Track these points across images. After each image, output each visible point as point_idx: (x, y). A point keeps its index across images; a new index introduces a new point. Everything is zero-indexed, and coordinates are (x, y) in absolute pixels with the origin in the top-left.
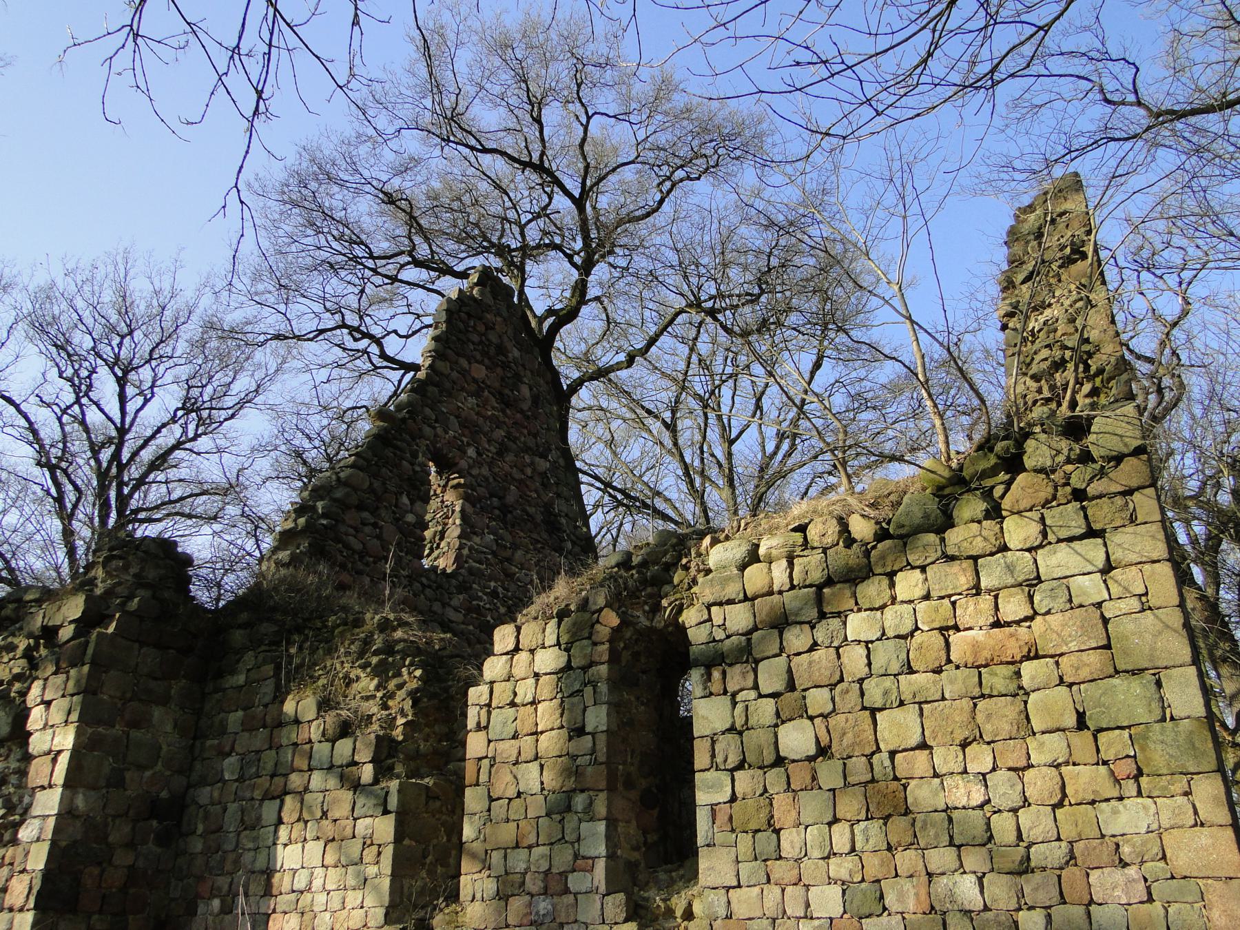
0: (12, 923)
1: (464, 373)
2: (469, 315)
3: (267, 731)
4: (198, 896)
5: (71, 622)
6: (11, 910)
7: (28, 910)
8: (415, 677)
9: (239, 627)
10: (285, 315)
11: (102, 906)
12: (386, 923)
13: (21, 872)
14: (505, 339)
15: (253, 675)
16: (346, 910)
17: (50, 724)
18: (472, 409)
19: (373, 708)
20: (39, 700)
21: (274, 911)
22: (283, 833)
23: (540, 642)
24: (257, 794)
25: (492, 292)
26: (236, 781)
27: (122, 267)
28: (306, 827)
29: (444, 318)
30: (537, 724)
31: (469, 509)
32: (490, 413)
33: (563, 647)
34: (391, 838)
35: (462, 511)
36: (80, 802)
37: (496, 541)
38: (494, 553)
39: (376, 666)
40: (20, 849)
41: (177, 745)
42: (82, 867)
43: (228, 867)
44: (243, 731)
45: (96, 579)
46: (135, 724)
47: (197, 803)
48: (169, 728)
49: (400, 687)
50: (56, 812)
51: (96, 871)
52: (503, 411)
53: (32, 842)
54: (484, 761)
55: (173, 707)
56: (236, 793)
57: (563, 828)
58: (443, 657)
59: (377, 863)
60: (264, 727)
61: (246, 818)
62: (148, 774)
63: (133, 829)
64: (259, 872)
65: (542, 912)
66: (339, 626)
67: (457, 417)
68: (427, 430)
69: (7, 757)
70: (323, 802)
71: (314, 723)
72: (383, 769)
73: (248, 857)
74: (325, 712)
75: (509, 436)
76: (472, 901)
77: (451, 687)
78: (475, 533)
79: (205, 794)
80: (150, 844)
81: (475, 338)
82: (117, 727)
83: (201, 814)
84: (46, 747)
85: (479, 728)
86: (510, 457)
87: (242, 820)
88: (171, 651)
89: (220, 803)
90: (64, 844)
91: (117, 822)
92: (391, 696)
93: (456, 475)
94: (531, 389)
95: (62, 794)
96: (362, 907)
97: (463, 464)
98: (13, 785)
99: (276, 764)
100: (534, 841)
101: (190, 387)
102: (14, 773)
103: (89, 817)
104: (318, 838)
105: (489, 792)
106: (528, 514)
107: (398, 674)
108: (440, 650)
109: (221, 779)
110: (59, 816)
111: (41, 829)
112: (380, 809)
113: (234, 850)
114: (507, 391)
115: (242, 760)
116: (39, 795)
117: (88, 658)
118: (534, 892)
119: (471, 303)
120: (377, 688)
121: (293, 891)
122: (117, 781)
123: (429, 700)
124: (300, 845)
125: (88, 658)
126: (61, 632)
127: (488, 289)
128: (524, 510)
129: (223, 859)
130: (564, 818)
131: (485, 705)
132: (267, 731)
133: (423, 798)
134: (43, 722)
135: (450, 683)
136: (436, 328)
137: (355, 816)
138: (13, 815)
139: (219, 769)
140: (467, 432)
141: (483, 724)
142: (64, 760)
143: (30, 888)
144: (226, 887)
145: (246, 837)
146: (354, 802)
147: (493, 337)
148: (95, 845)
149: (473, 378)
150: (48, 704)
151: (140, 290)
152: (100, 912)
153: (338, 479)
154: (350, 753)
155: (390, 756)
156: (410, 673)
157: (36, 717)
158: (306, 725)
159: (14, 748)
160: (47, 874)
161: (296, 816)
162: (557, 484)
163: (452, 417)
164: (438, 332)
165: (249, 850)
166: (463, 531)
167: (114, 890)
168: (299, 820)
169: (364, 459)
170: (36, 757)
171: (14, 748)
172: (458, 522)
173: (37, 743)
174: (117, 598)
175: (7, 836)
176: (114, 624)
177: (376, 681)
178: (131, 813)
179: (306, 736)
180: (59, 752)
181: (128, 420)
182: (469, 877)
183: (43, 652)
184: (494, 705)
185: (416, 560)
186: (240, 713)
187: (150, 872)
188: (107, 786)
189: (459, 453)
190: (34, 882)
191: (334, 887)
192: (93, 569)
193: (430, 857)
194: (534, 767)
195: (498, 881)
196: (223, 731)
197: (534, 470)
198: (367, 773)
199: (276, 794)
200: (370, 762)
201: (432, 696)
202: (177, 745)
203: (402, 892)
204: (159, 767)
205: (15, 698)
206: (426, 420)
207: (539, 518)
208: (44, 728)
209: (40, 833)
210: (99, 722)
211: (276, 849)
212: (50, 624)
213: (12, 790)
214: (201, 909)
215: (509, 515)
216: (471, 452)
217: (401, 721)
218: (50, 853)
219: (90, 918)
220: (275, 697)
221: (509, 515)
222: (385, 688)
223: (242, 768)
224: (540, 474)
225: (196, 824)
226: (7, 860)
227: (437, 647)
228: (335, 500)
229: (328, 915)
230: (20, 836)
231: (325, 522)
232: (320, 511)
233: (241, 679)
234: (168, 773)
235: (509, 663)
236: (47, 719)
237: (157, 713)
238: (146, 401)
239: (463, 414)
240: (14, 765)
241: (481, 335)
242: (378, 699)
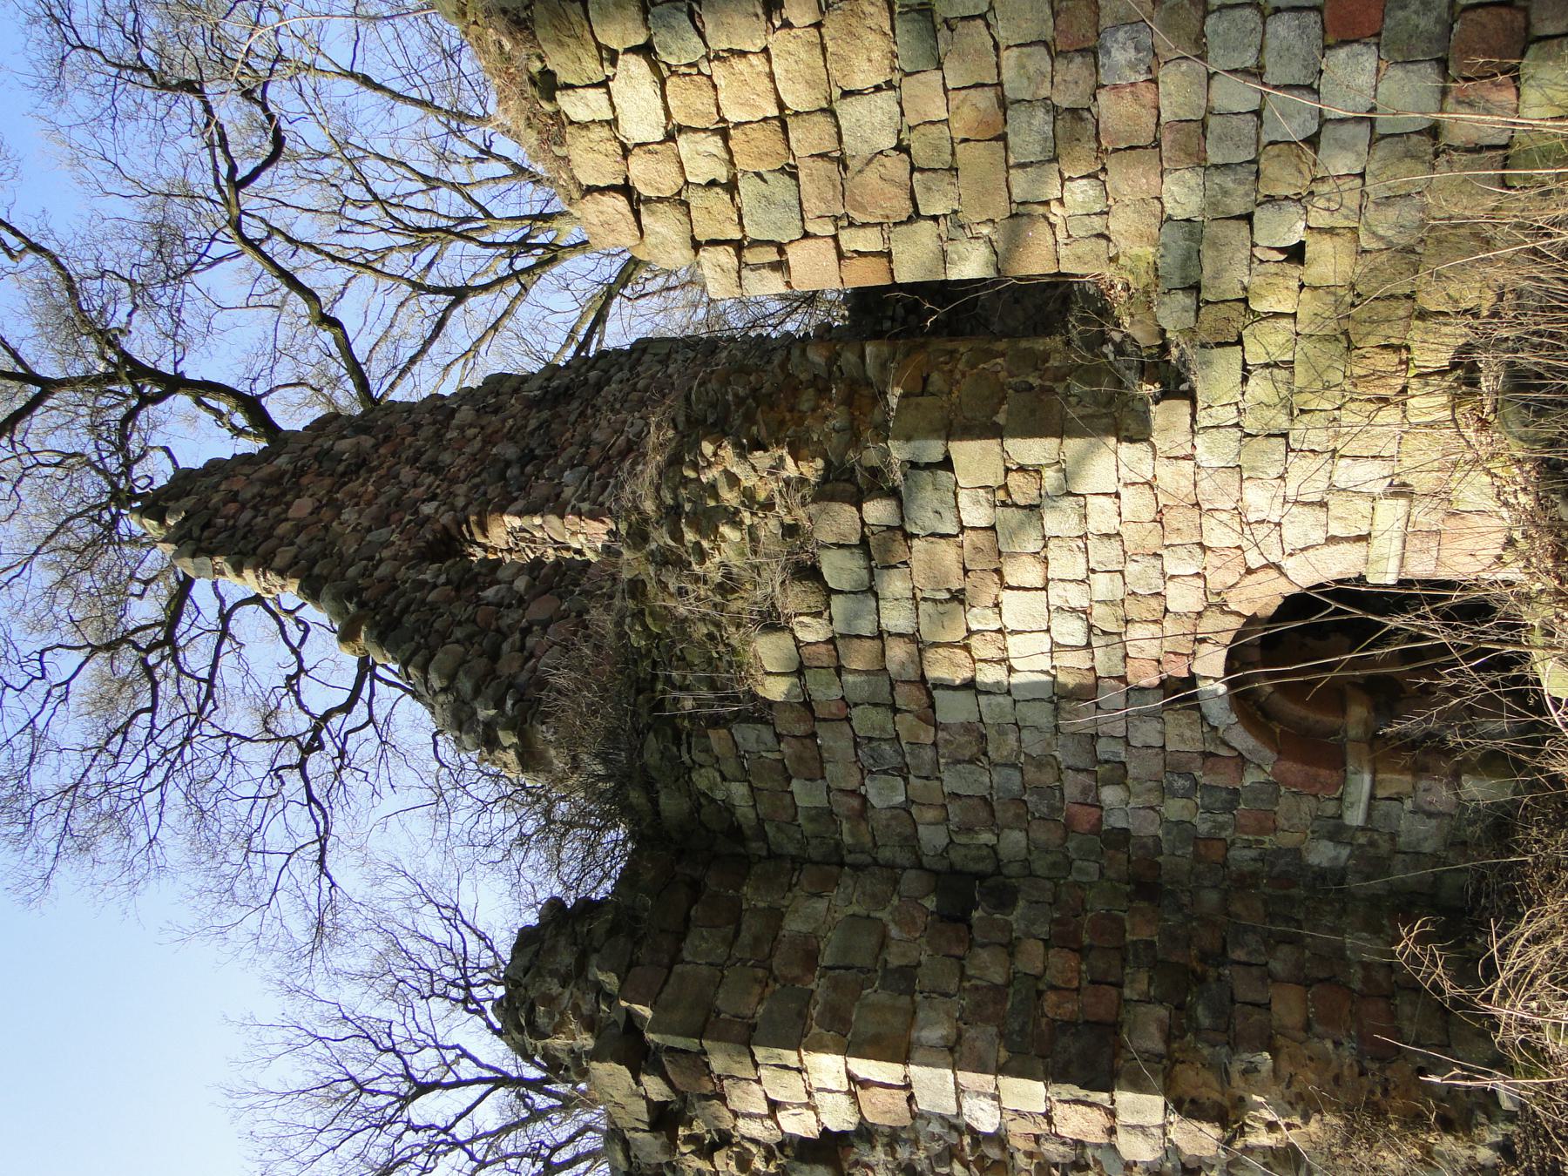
0: (1133, 1127)
1: (299, 528)
2: (207, 525)
3: (821, 729)
4: (1096, 829)
5: (638, 1083)
6: (1112, 1131)
7: (1113, 1102)
8: (715, 454)
9: (654, 802)
10: (290, 855)
11: (1111, 984)
12: (1147, 440)
13: (1050, 1121)
14: (255, 476)
15: (730, 768)
16: (1122, 529)
17: (805, 1099)
18: (360, 513)
19: (769, 528)
20: (769, 1123)
21: (1122, 679)
22: (990, 675)
23: (605, 132)
24: (927, 735)
25: (178, 499)
26: (906, 780)
27: (253, 1100)
28: (978, 632)
29: (206, 560)
30: (765, 119)
31: (520, 504)
32: (371, 488)
33: (609, 71)
34: (993, 445)
35: (520, 514)
36: (934, 1033)
37: (573, 467)
38: (592, 469)
39: (699, 531)
40: (1012, 1127)
41: (850, 890)
42: (1044, 1020)
43: (1048, 778)
44: (823, 778)
45: (572, 1051)
46: (810, 958)
47: (946, 849)
48: (821, 905)
49: (733, 480)
50: (949, 1072)
51: (1051, 998)
52: (372, 470)
53: (1001, 1109)
54: (846, 246)
55: (786, 903)
56: (927, 778)
57: (963, 18)
58: (688, 417)
59: (1038, 471)
60: (814, 736)
61: (967, 754)
62: (894, 931)
63: (983, 946)
64: (1056, 717)
65: (1132, 54)
66: (646, 627)
67: (369, 530)
68: (383, 570)
69: (868, 1166)
70: (935, 601)
71: (799, 635)
72: (875, 484)
73: (1033, 744)
74: (779, 617)
75: (413, 461)
76: (1108, 239)
77: (736, 395)
78: (558, 496)
79: (932, 837)
80: (1011, 918)
81: (246, 515)
82: (813, 986)
83: (961, 839)
84: (845, 1101)
85: (781, 266)
86: (446, 457)
87: (971, 761)
88: (693, 912)
89: (944, 806)
90: (1004, 1055)
91: (971, 972)
92: (749, 496)
93: (464, 527)
94: (344, 437)
95: (918, 1064)
96: (1117, 495)
97: (446, 519)
98: (912, 1153)
99: (876, 705)
100: (990, 93)
101: (433, 994)
102: (893, 1153)
103: (960, 1018)
104: (997, 605)
105: (901, 223)
106: (539, 428)
107: (712, 488)
108: (675, 428)
109: (906, 808)
110: (955, 1067)
111: (979, 1094)
112: (943, 475)
113: (1021, 770)
114: (341, 468)
115: (870, 772)
116: (923, 1105)
117: (692, 1044)
118: (1092, 82)
119: (188, 525)
120: (736, 524)
121: (1089, 645)
122: (905, 978)
123: (755, 423)
124: (1010, 640)
125: (692, 1044)
126: (655, 1098)
127: (170, 504)
128: (532, 433)
129: (1038, 790)
130: (946, 21)
131: (739, 255)
132: (821, 729)
133: (925, 401)
134: (804, 1111)
135: (730, 397)
136: (222, 573)
137: (954, 530)
138: (963, 1149)
139: (889, 814)
140: (396, 517)
141: (771, 255)
142: (865, 1068)
143: (1077, 1102)
144: (1082, 777)
145: (998, 749)
146: (933, 535)
147: (247, 494)
148: (1009, 1005)
149: (312, 513)
150: (774, 1106)
151: (296, 1072)
152: (1119, 985)
153: (444, 690)
154: (846, 552)
155: (851, 479)
156: (710, 465)
157: (799, 1124)
158: (806, 651)
159: (852, 1157)
160: (1054, 1074)
161: (961, 655)
162: (498, 394)
163: (368, 538)
164: (227, 568)
165: (1019, 740)
166: (552, 512)
167: (1084, 967)
168: (967, 648)
169: (414, 653)
170: (863, 1117)
171: (852, 1157)
172: (537, 520)
173: (839, 1117)
174: (599, 1010)
175: (994, 1153)
176: (636, 1007)
177: (725, 530)
178: (958, 951)
179: (823, 649)
180: (851, 1077)
181: (487, 1074)
182: (1063, 251)
183: (699, 1127)
184: (738, 236)
185: (591, 570)
186: (795, 785)
187: (1057, 915)
188: (912, 993)
189: (428, 526)
190: (1066, 1096)
191: (1081, 558)
192: (556, 1057)
193: (1031, 380)
194: (849, 112)
195: (1071, 179)
196: (827, 815)
197: (471, 426)
198: (878, 511)
199: (925, 700)
200: (860, 510)
201: (749, 419)
202: (850, 890)
203: (1092, 416)
204: (884, 915)
205: (779, 1166)
206: (365, 573)
207: (546, 414)
208: (814, 1108)
209: (985, 1095)
210: (802, 1016)
211: (1017, 686)
212: (646, 1118)
213: (922, 1154)
214: (1117, 821)
215: (537, 452)
216: (427, 509)
217: (791, 469)
218: (1019, 1076)
219: (1128, 1001)
220: (762, 720)
221: (537, 452)
222: (737, 511)
223: (885, 772)
224: (479, 417)
225: (979, 847)
226: (1031, 1146)
227: (671, 433)
228: (477, 692)
229: (1131, 568)
230: (991, 1130)
231: (509, 703)
232: (492, 712)
233: (739, 791)
234: (895, 901)
235: (653, 206)
236: (800, 1105)
237: (794, 925)
238: (465, 1054)
239: (366, 524)
240: (879, 1155)
241: (243, 507)
242: (756, 520)
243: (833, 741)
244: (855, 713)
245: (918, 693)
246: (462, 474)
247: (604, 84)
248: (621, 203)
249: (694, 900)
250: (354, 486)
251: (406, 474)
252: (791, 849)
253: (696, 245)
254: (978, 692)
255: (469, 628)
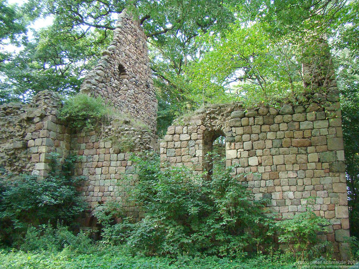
23: (182, 132)
48: (64, 147)
85: (164, 153)
128: (141, 82)
171: (22, 150)
243: (93, 151)
244: (97, 156)
245: (101, 165)
246: (134, 69)
247: (187, 133)
248: (173, 133)
249: (65, 126)
250: (133, 47)
251: (135, 57)
252: (73, 142)
253: (167, 142)
254: (101, 175)
255: (107, 76)
